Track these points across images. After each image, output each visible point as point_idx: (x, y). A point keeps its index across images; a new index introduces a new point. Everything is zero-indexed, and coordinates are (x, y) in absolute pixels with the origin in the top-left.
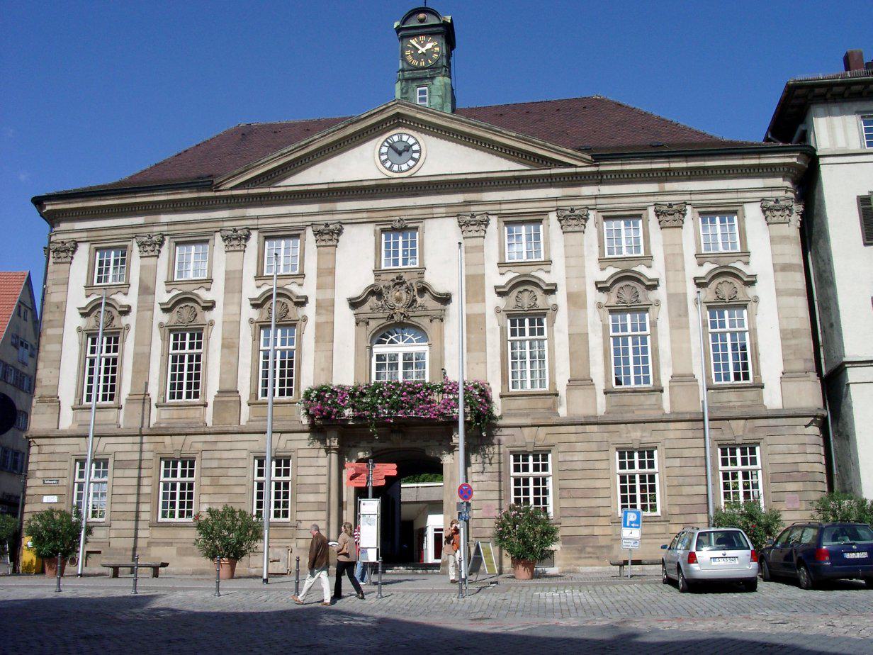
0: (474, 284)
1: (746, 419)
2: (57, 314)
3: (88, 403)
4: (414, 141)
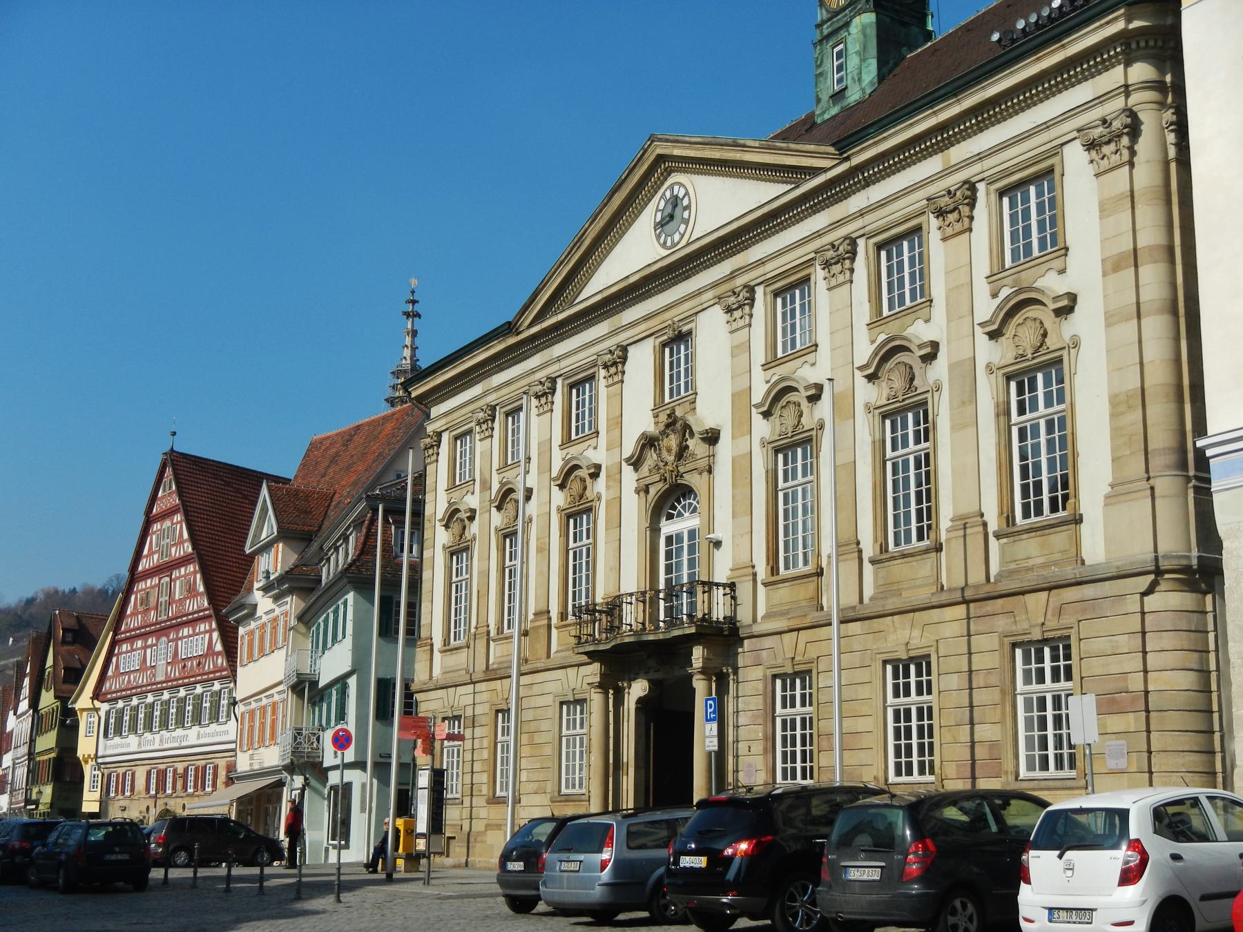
0: (741, 398)
1: (1050, 589)
3: (509, 631)
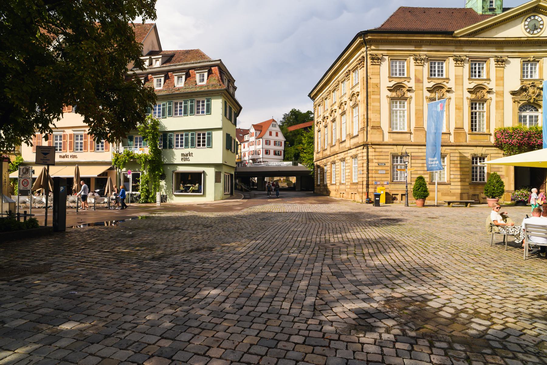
2: (376, 89)
4: (541, 19)
